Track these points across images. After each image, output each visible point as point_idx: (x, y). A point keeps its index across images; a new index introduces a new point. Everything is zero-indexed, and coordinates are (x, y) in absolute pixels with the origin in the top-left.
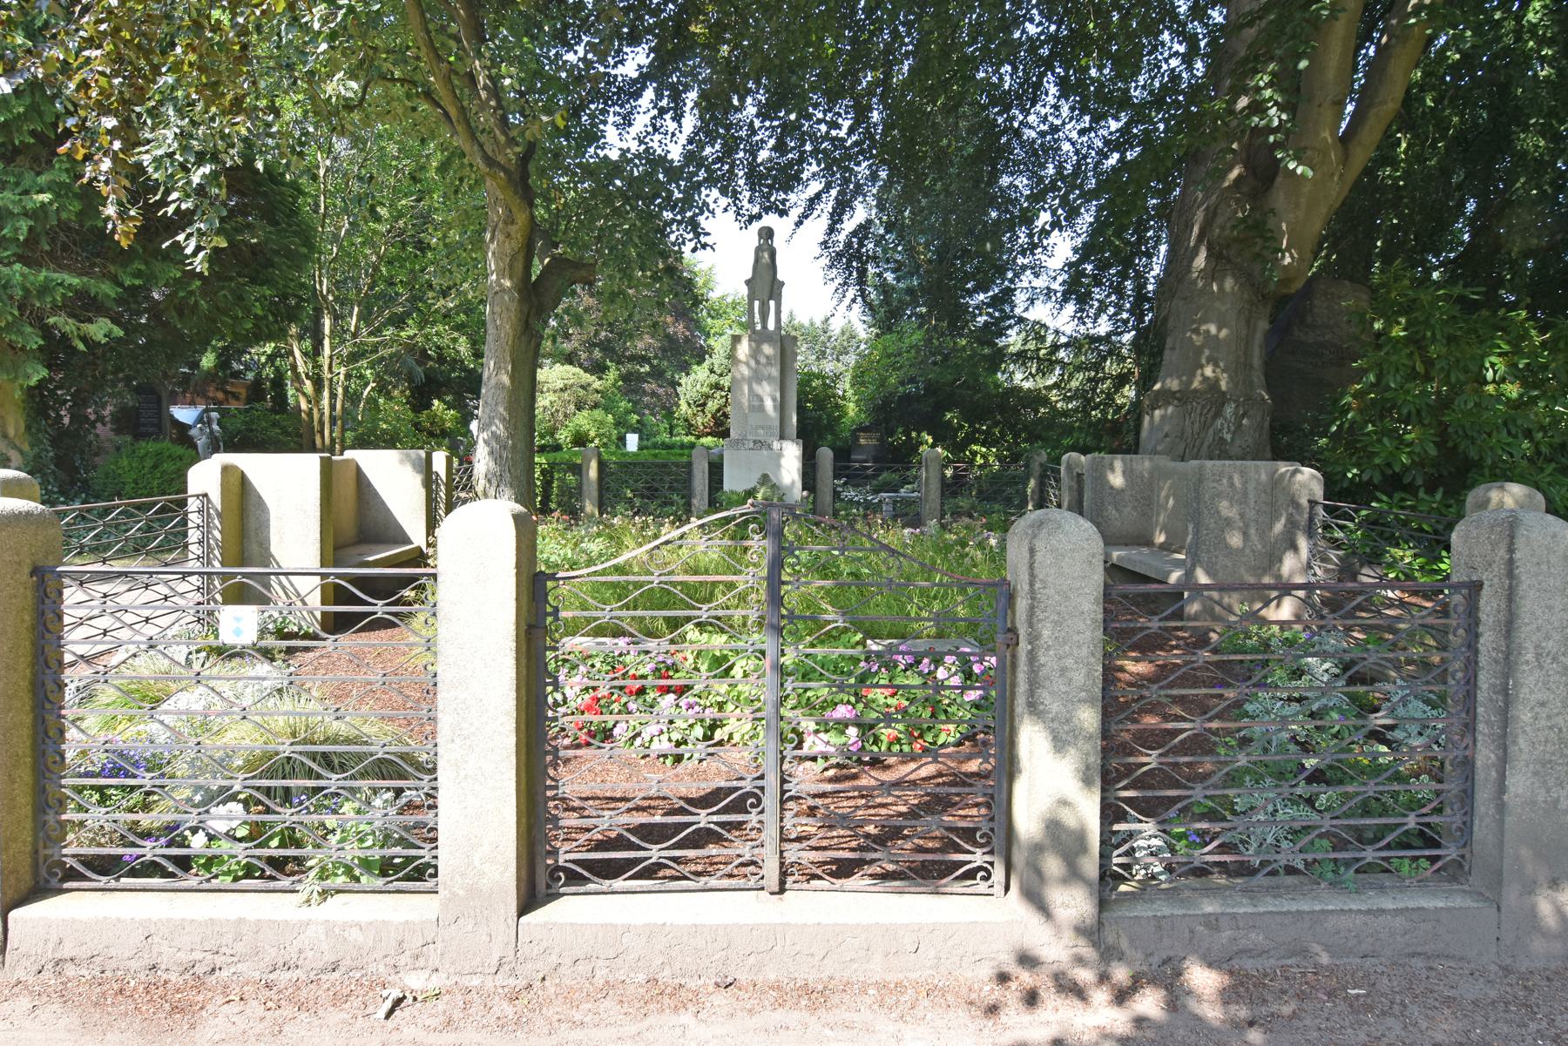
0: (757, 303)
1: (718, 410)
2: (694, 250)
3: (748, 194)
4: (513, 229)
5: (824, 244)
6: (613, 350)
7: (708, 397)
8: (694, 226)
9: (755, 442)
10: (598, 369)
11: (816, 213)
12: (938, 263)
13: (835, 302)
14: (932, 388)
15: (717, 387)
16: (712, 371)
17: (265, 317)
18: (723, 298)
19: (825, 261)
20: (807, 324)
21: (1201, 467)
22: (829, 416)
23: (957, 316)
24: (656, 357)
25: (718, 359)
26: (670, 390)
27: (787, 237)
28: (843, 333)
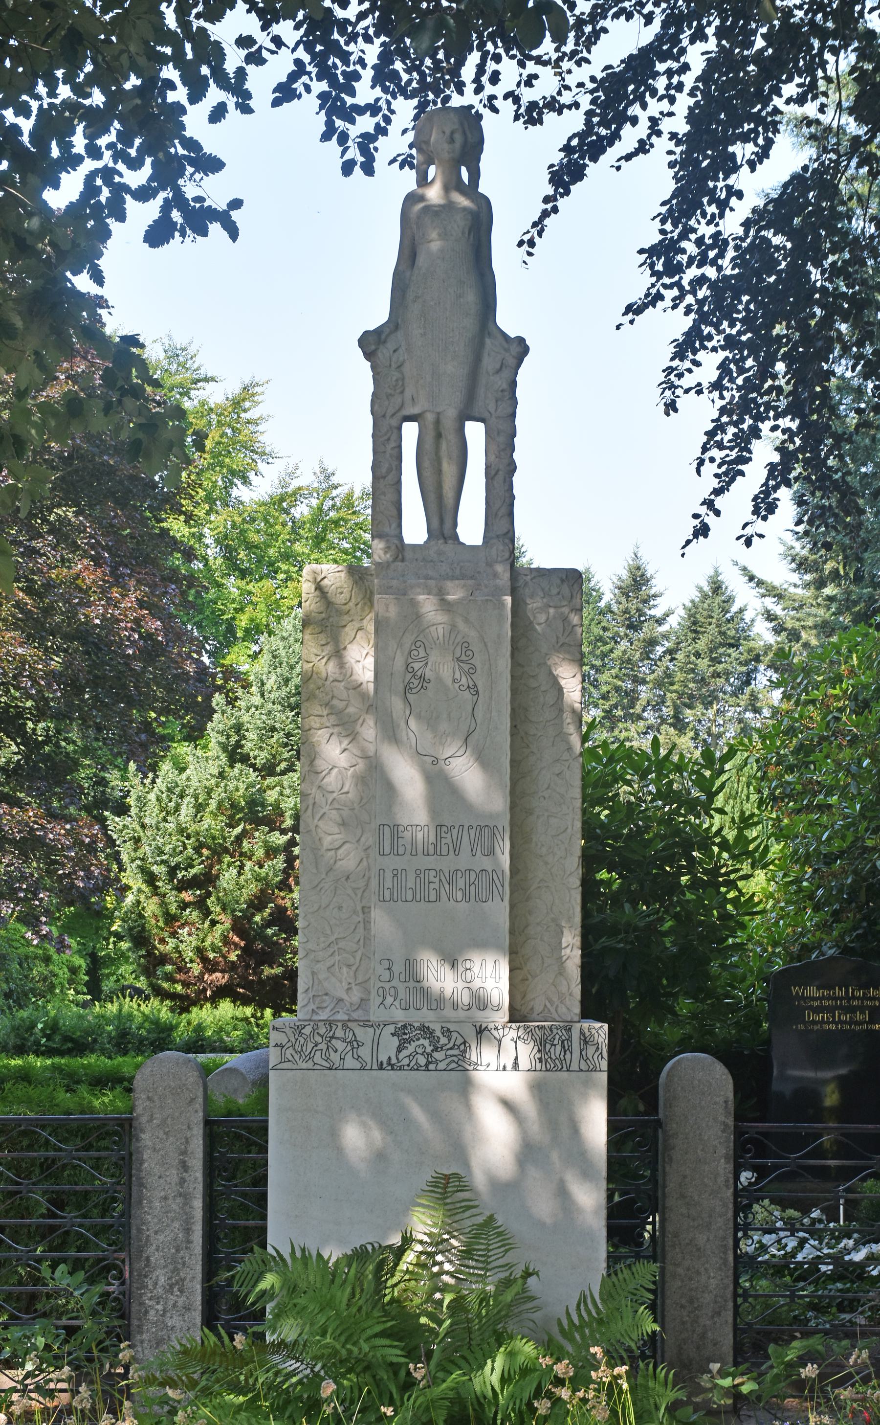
0: (410, 432)
1: (258, 903)
2: (158, 235)
3: (372, 52)
5: (663, 256)
7: (218, 852)
9: (403, 1033)
11: (630, 136)
13: (709, 481)
15: (255, 813)
16: (235, 755)
18: (282, 502)
19: (670, 323)
22: (685, 920)
24: (40, 714)
25: (252, 712)
26: (89, 832)
28: (695, 624)
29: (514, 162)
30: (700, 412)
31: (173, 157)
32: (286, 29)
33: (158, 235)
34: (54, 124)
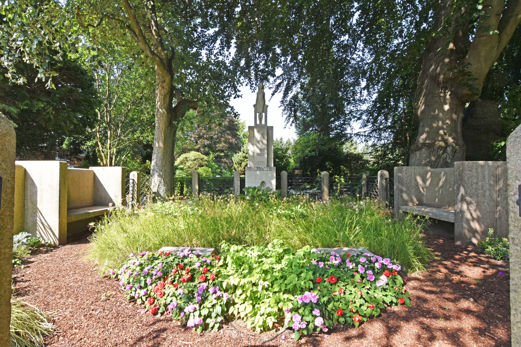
0: (258, 114)
2: (235, 98)
4: (165, 84)
5: (282, 102)
6: (212, 148)
7: (242, 161)
8: (235, 88)
10: (207, 154)
11: (279, 91)
12: (321, 110)
13: (286, 122)
14: (321, 153)
17: (79, 125)
19: (283, 108)
21: (463, 164)
23: (326, 130)
24: (226, 150)
27: (269, 99)
28: (287, 143)
29: (268, 92)
30: (285, 116)
32: (246, 80)
33: (235, 98)
34: (225, 88)
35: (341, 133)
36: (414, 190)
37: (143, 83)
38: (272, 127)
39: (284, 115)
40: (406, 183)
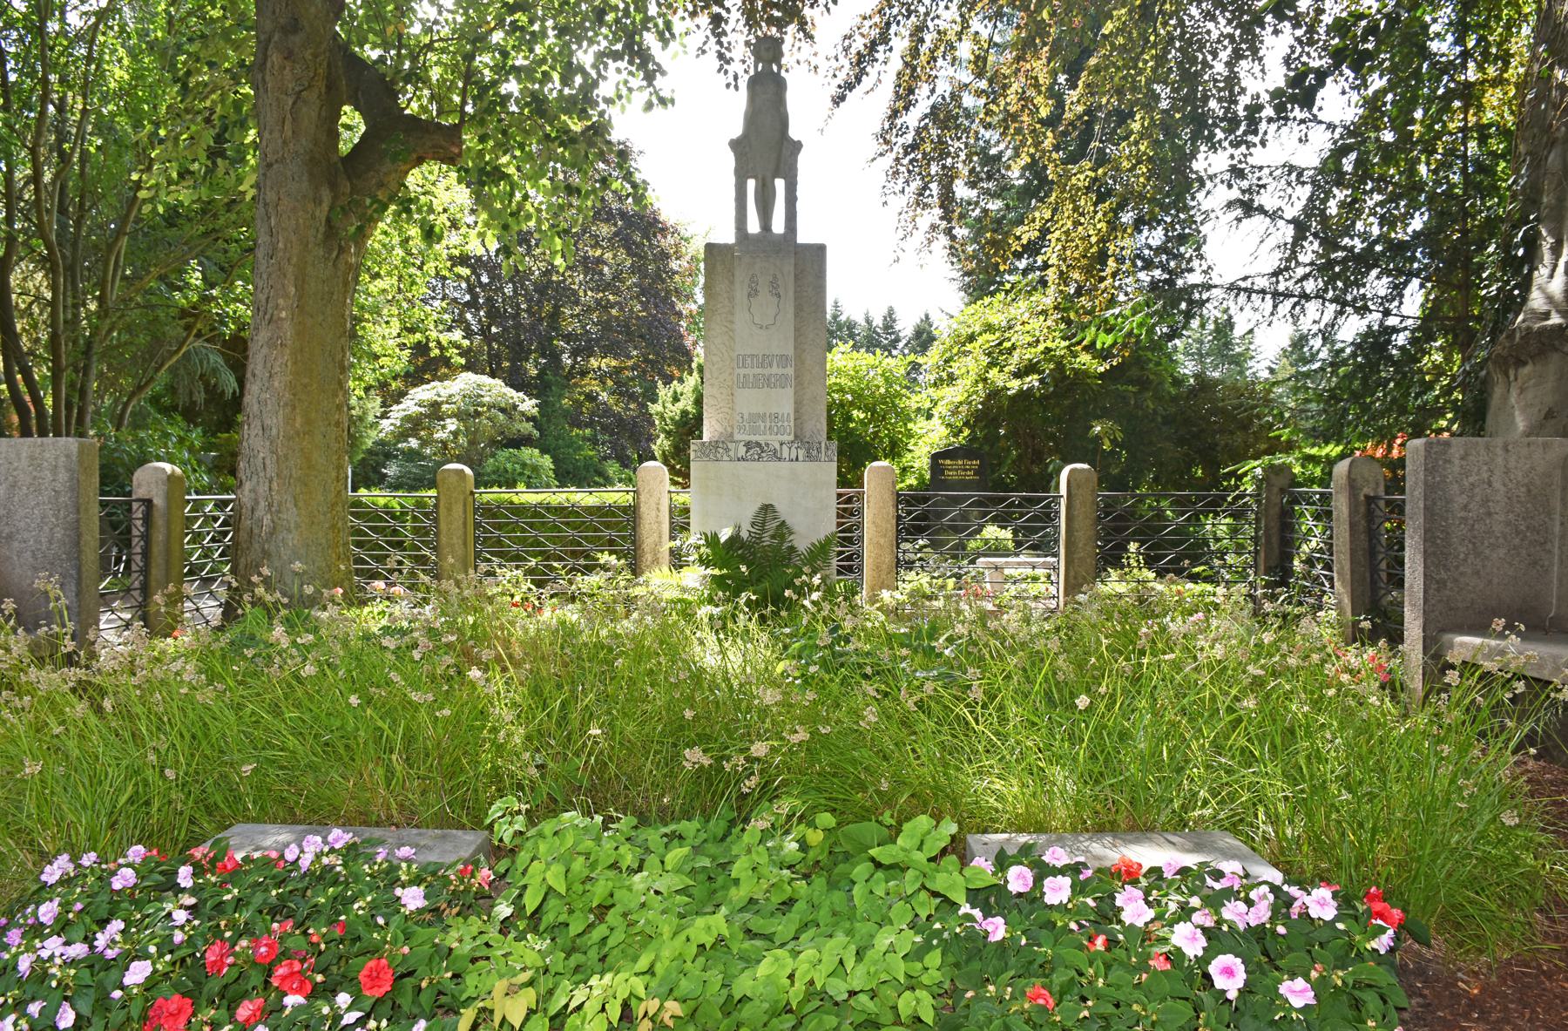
0: (751, 184)
2: (649, 106)
9: (748, 445)
11: (867, 82)
19: (889, 160)
20: (861, 321)
31: (649, 69)
33: (649, 106)
35: (1170, 282)
36: (1502, 552)
37: (1268, 638)
38: (820, 250)
39: (891, 199)
40: (1465, 519)
